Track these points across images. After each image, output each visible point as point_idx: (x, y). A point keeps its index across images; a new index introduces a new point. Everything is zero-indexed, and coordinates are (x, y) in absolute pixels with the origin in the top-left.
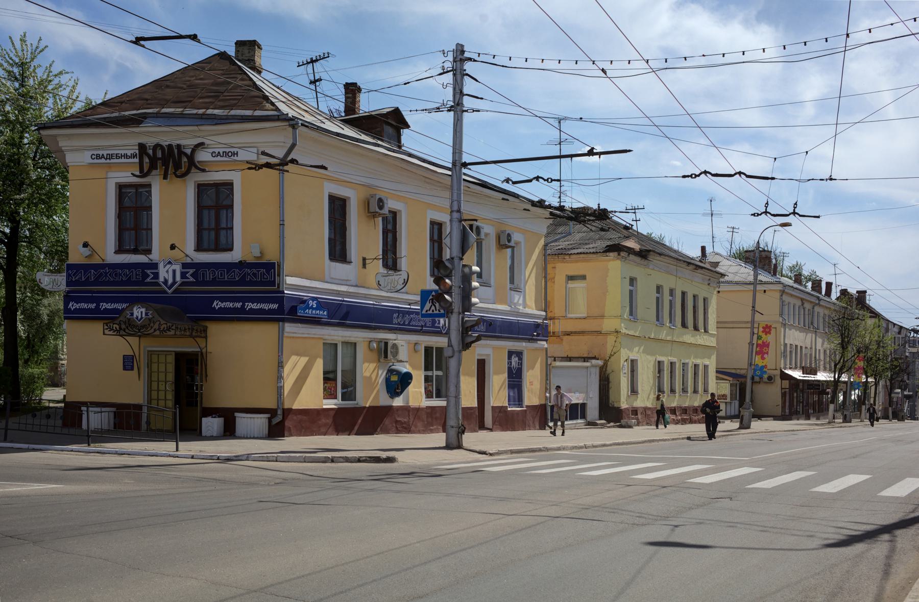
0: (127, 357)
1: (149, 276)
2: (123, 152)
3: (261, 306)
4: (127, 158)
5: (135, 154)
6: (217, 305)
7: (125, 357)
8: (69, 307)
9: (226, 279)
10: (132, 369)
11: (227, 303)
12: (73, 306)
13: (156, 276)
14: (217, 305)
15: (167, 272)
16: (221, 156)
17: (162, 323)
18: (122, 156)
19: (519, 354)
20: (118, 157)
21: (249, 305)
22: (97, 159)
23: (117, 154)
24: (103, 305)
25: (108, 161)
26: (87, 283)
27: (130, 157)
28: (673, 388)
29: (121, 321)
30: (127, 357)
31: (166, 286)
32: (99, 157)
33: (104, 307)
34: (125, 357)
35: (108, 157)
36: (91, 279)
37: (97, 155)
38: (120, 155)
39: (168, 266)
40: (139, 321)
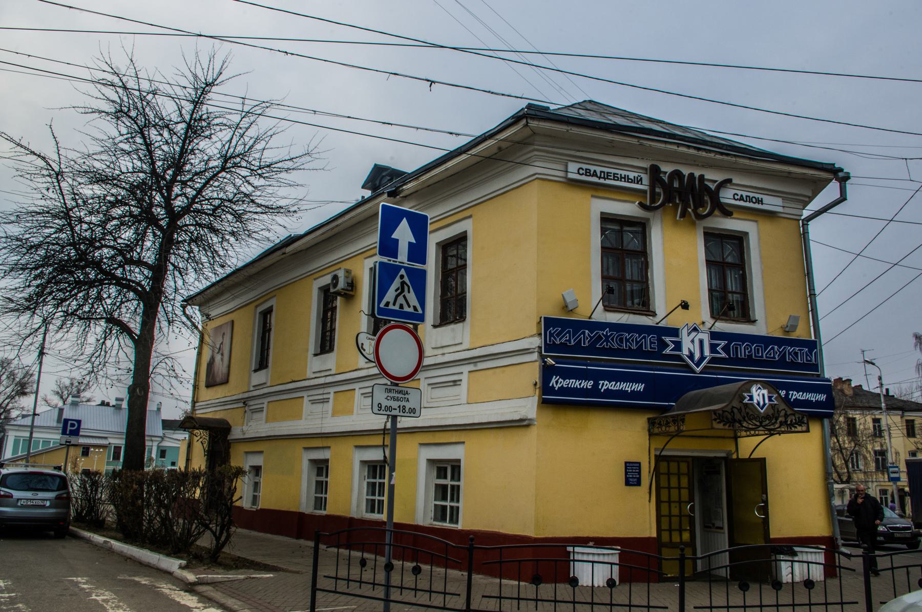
0: (631, 465)
1: (668, 346)
2: (623, 173)
3: (621, 387)
4: (628, 182)
5: (639, 178)
6: (557, 384)
7: (628, 465)
8: (551, 385)
9: (765, 358)
10: (638, 483)
11: (571, 381)
12: (557, 382)
13: (678, 346)
14: (557, 384)
15: (692, 341)
16: (744, 201)
17: (788, 413)
18: (621, 178)
19: (455, 467)
20: (616, 178)
21: (605, 383)
22: (586, 175)
23: (614, 174)
24: (603, 384)
25: (602, 181)
26: (578, 348)
27: (632, 181)
28: (841, 499)
29: (733, 407)
30: (631, 465)
31: (692, 360)
32: (590, 173)
33: (605, 387)
34: (628, 465)
35: (602, 176)
36: (584, 344)
37: (586, 169)
38: (619, 176)
39: (694, 334)
40: (762, 409)
